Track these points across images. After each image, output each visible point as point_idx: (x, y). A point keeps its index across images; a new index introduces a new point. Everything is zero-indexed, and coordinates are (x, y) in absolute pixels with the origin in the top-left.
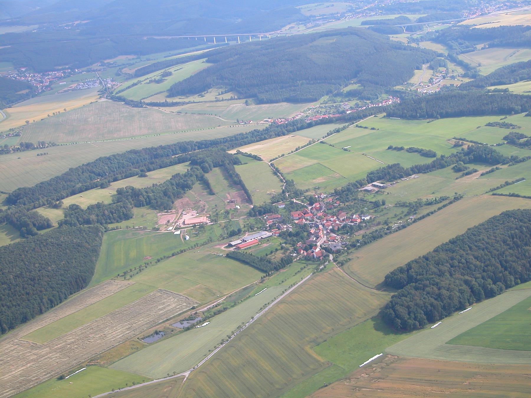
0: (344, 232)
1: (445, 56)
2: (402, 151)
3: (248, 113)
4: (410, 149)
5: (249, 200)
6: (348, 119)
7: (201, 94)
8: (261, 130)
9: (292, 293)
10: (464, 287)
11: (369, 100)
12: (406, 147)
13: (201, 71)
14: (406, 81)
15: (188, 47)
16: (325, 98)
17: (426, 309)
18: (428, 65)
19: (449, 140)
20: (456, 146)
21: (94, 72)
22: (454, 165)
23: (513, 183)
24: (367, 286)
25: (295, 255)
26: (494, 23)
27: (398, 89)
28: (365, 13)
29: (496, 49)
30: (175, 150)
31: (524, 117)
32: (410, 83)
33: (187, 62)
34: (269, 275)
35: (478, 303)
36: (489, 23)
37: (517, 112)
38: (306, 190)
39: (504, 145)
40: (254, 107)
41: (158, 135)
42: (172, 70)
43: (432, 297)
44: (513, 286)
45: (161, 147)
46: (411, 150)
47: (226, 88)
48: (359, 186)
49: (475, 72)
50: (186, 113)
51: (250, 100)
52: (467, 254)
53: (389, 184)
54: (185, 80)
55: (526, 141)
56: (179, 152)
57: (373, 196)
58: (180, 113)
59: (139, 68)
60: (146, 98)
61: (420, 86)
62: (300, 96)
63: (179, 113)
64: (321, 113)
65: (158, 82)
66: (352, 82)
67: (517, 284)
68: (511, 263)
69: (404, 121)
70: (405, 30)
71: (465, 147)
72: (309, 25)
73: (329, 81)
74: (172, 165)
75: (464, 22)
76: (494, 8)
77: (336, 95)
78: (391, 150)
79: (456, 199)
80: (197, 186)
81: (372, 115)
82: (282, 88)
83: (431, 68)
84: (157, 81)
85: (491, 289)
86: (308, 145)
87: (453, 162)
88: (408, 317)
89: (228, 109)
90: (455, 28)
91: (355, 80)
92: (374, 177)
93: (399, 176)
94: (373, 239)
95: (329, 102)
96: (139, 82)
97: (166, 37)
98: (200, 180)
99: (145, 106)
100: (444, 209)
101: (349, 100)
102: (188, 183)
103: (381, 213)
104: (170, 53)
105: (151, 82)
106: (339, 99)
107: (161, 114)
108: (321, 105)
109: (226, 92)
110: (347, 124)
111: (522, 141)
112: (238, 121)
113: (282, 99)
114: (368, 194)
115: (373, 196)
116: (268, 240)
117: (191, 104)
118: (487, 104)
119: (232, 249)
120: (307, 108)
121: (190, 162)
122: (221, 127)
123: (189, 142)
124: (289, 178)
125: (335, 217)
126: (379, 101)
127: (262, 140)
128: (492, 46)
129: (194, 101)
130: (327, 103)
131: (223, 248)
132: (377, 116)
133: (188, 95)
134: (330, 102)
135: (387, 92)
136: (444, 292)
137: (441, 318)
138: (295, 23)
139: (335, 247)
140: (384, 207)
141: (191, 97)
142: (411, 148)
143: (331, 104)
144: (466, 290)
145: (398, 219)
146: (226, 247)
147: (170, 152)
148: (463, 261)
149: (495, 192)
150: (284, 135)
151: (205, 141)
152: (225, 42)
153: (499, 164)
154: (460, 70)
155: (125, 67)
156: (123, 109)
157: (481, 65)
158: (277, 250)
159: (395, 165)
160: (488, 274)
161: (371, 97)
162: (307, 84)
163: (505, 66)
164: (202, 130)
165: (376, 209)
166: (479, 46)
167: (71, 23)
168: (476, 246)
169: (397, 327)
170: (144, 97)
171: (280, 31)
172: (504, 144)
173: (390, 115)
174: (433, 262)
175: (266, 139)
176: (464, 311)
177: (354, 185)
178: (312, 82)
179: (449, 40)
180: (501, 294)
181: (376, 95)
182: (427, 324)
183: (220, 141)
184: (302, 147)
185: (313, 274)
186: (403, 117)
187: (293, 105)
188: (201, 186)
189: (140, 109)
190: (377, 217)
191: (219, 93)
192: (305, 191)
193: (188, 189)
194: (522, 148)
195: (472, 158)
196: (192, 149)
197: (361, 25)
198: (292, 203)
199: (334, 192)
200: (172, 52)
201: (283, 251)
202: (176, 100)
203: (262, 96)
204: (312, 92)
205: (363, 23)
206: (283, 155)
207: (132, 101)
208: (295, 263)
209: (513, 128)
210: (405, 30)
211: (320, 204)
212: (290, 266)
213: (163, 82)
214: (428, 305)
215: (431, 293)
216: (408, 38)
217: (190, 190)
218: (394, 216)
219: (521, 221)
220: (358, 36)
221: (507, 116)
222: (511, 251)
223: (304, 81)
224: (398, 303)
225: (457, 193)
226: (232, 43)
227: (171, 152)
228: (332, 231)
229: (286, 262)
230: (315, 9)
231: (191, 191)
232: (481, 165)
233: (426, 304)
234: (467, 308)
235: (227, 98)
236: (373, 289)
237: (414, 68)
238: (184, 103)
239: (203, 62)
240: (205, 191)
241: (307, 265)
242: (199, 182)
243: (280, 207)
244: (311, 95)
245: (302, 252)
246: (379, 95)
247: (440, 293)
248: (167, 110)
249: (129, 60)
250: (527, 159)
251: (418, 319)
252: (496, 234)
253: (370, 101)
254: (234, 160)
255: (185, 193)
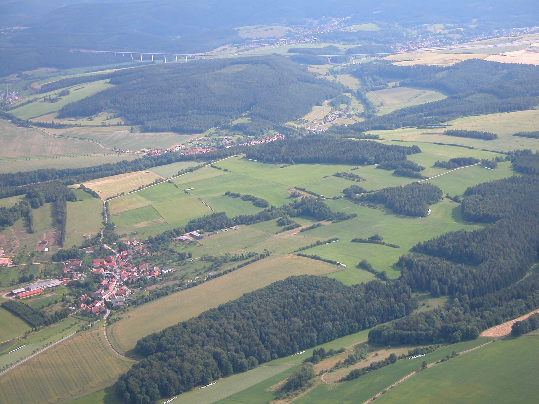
0: (137, 285)
1: (354, 92)
2: (238, 198)
3: (130, 141)
4: (246, 196)
5: (60, 242)
6: (207, 157)
7: (91, 117)
8: (130, 161)
9: (42, 354)
10: (211, 360)
11: (254, 136)
12: (243, 194)
13: (99, 93)
14: (300, 117)
15: (112, 64)
16: (212, 130)
17: (162, 383)
18: (329, 101)
19: (289, 189)
20: (293, 196)
21: (5, 84)
22: (280, 218)
23: (325, 242)
24: (118, 352)
25: (74, 308)
26: (414, 60)
27: (287, 125)
28: (299, 39)
29: (406, 88)
30: (34, 178)
31: (375, 169)
32: (303, 120)
33: (93, 81)
34: (36, 330)
35: (225, 377)
36: (409, 60)
37: (370, 163)
38: (122, 235)
39: (341, 199)
40: (138, 135)
41: (28, 159)
42: (72, 90)
43: (172, 370)
44: (269, 361)
45: (20, 174)
46: (247, 198)
47: (116, 113)
48: (175, 234)
49: (374, 112)
50: (68, 137)
51: (136, 127)
52: (229, 323)
53: (207, 234)
54: (79, 101)
55: (362, 197)
56: (39, 180)
57: (184, 247)
58: (63, 136)
59: (46, 84)
60: (35, 117)
61: (313, 123)
62: (187, 126)
63: (61, 136)
64: (201, 146)
65: (52, 101)
66: (244, 115)
67: (273, 358)
68: (271, 335)
69: (260, 164)
70: (329, 61)
71: (299, 199)
72: (242, 48)
73: (220, 112)
74: (9, 197)
75: (389, 56)
76: (429, 43)
77: (223, 128)
78: (228, 196)
79: (262, 256)
80: (20, 222)
81: (233, 155)
82: (171, 116)
83: (332, 104)
84: (51, 100)
85: (241, 363)
86: (153, 184)
87: (280, 214)
88: (139, 390)
89: (111, 136)
90: (376, 63)
91: (247, 113)
92: (194, 225)
93: (219, 226)
94: (156, 296)
95: (214, 135)
96: (36, 100)
97: (93, 51)
98: (25, 216)
99: (30, 126)
100: (245, 267)
101: (234, 134)
102: (8, 219)
103: (183, 267)
104: (92, 69)
105: (46, 100)
106: (225, 132)
107: (43, 136)
108: (205, 138)
109: (115, 117)
110: (203, 163)
111: (359, 195)
112: (115, 149)
113: (169, 128)
114: (180, 244)
115: (184, 247)
116: (53, 290)
117: (77, 127)
118: (344, 152)
119: (11, 298)
120: (190, 140)
121: (26, 195)
122: (95, 155)
123: (50, 170)
124: (113, 220)
125: (136, 268)
126: (264, 137)
127: (116, 174)
128: (402, 85)
129: (80, 124)
130: (211, 136)
131: (4, 296)
132: (237, 157)
133: (78, 117)
134: (215, 135)
135: (275, 128)
136: (186, 365)
137: (178, 393)
138: (229, 45)
139: (117, 302)
140: (189, 260)
141: (81, 120)
142: (247, 195)
143: (215, 138)
144: (211, 363)
145: (197, 275)
146: (8, 295)
147: (28, 179)
148: (222, 330)
149: (300, 252)
150: (141, 171)
151: (68, 169)
152: (152, 60)
153: (325, 220)
154: (361, 109)
155: (35, 81)
156: (7, 128)
157: (384, 104)
158: (56, 302)
159: (219, 214)
160: (242, 347)
161: (256, 133)
162: (198, 114)
163: (404, 108)
164: (72, 157)
165: (180, 262)
166: (391, 84)
167: (10, 28)
168: (242, 315)
169: (126, 401)
170: (32, 116)
171: (211, 52)
172: (341, 197)
173: (250, 157)
174: (190, 330)
175: (121, 173)
176: (206, 386)
177: (171, 233)
178: (203, 112)
179: (366, 75)
180: (253, 369)
181: (262, 131)
182: (159, 399)
183: (83, 171)
184: (147, 186)
185: (77, 332)
186: (260, 159)
187: (178, 135)
188: (24, 222)
189: (25, 129)
190: (178, 270)
191: (107, 117)
192: (121, 236)
193: (8, 226)
194: (356, 203)
195: (300, 212)
196: (52, 177)
197: (288, 52)
198: (102, 248)
199: (148, 240)
200: (94, 68)
201: (63, 303)
202: (65, 121)
203: (149, 124)
204: (200, 123)
205: (290, 51)
206: (123, 193)
207: (19, 120)
208: (71, 317)
209: (358, 181)
210: (329, 61)
211: (128, 252)
212: (63, 320)
213: (57, 101)
214: (164, 378)
215: (172, 365)
216: (329, 69)
217: (10, 226)
218: (194, 271)
219: (300, 289)
220: (269, 65)
221: (359, 167)
222: (276, 323)
223: (195, 111)
224: (133, 374)
225: (267, 250)
226: (159, 62)
227: (29, 179)
228: (126, 283)
229: (61, 316)
230: (254, 32)
231: (10, 228)
232: (307, 219)
233: (163, 377)
234: (210, 383)
235: (114, 124)
236: (123, 355)
237: (314, 104)
238: (70, 126)
239: (105, 83)
240: (26, 228)
241: (79, 321)
242: (23, 218)
243: (87, 252)
244: (198, 126)
245: (82, 305)
246: (265, 131)
247: (181, 366)
248: (50, 132)
249: (48, 73)
250: (352, 216)
251: (149, 394)
252: (268, 303)
253: (254, 137)
254: (69, 195)
255: (3, 229)
